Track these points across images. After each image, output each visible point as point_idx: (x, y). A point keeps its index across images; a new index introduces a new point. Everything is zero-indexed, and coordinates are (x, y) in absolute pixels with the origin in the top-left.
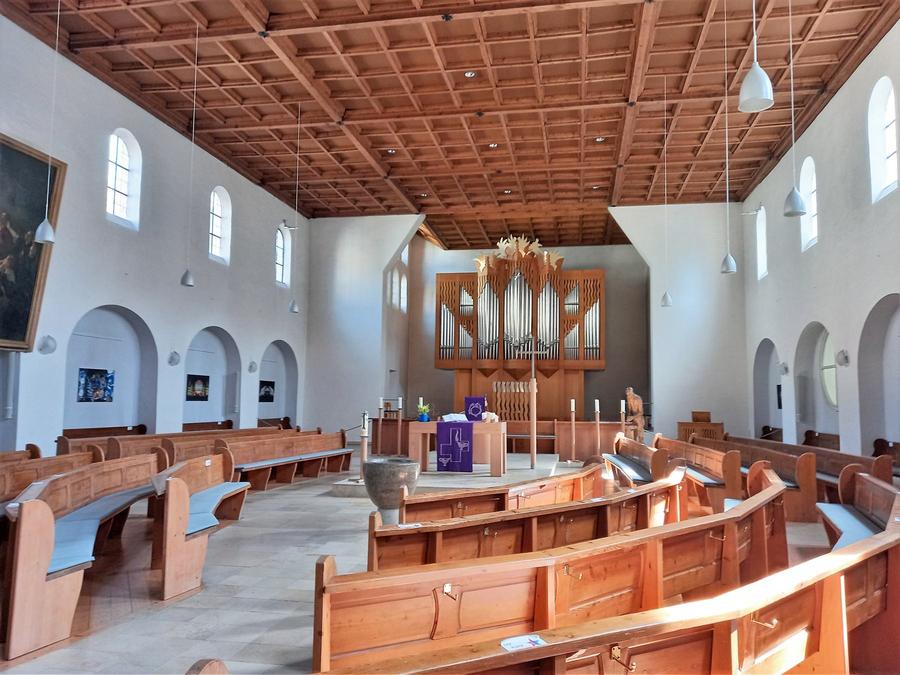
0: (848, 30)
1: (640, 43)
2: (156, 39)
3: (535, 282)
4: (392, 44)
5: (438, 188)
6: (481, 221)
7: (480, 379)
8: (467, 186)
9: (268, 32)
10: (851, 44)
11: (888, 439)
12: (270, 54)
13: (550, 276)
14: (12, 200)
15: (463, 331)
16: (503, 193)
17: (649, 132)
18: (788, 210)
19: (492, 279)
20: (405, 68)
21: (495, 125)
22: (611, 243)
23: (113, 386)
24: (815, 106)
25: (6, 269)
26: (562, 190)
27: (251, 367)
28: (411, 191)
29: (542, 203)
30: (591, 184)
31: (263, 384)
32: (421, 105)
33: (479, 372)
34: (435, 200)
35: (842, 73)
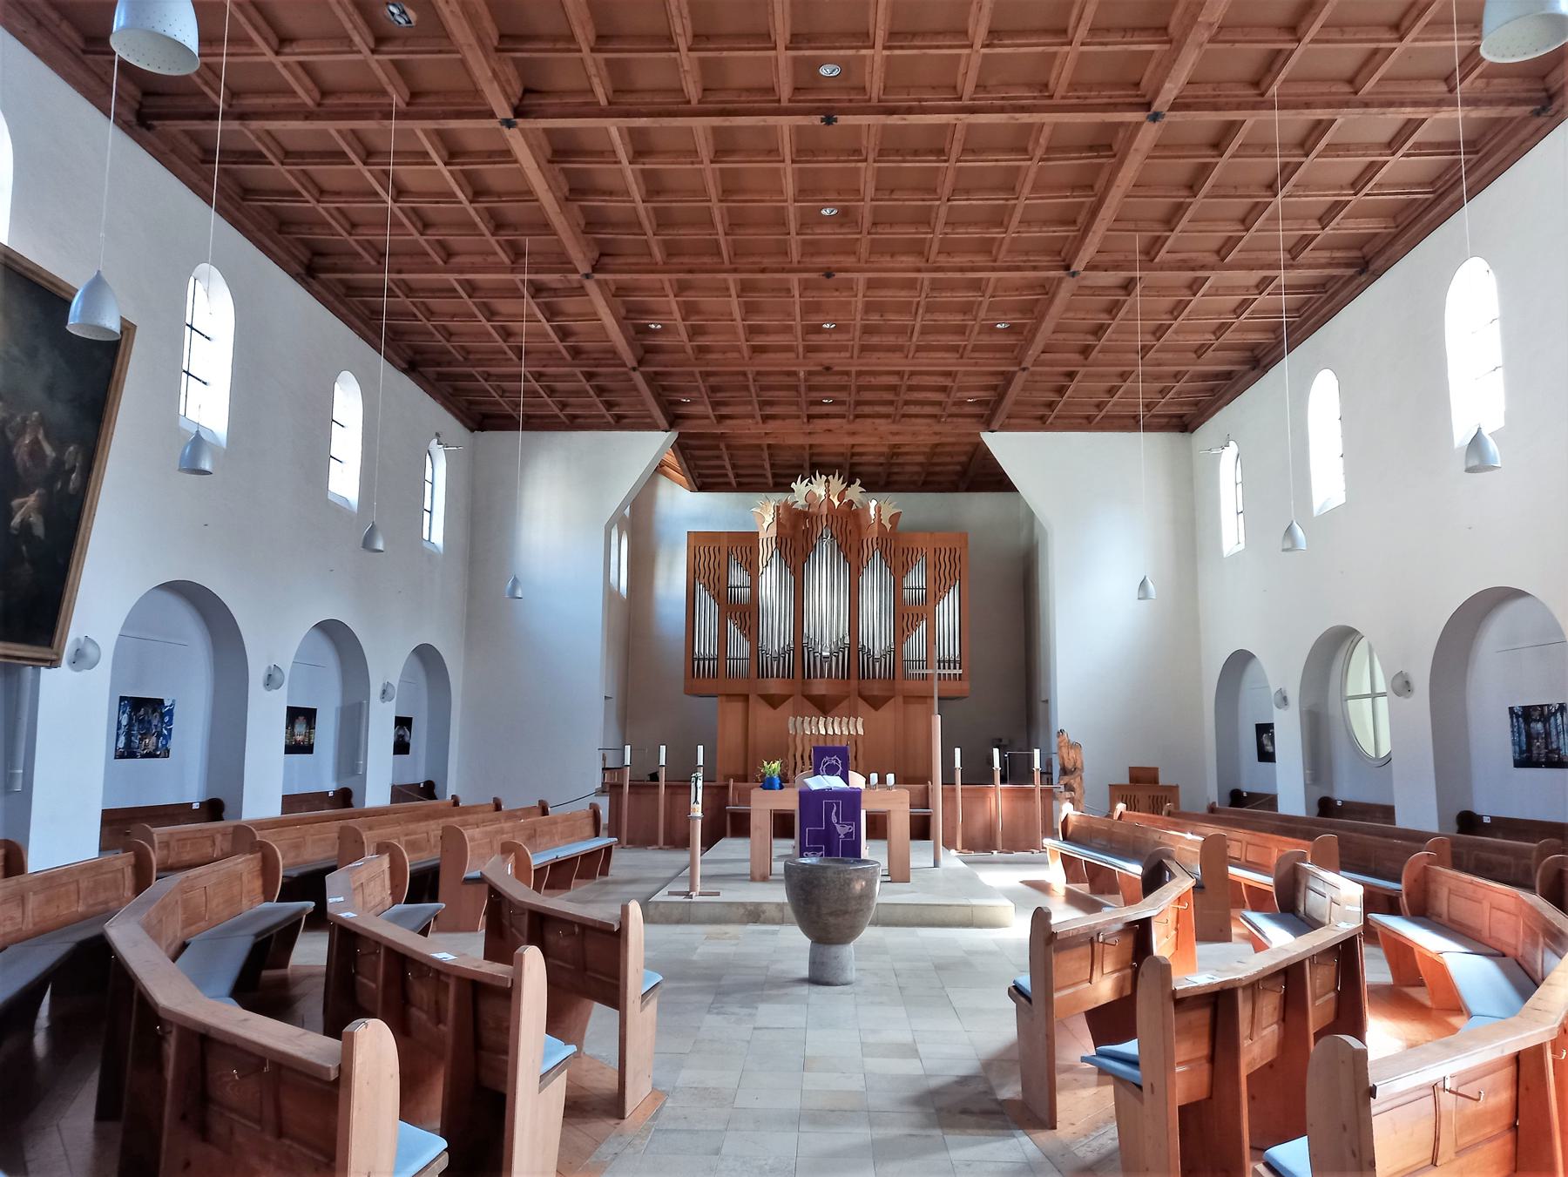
0: (1419, 185)
1: (1118, 182)
2: (309, 116)
3: (854, 550)
4: (719, 154)
5: (714, 389)
6: (769, 446)
7: (761, 712)
8: (763, 388)
9: (517, 120)
10: (1420, 205)
11: (1478, 810)
12: (506, 155)
13: (880, 541)
14: (50, 390)
17: (1084, 319)
18: (1474, 462)
20: (726, 193)
21: (844, 294)
22: (968, 490)
23: (171, 729)
24: (1344, 293)
25: (32, 515)
27: (384, 692)
28: (667, 393)
29: (877, 421)
31: (294, 714)
32: (732, 254)
33: (760, 699)
34: (705, 409)
35: (1398, 246)
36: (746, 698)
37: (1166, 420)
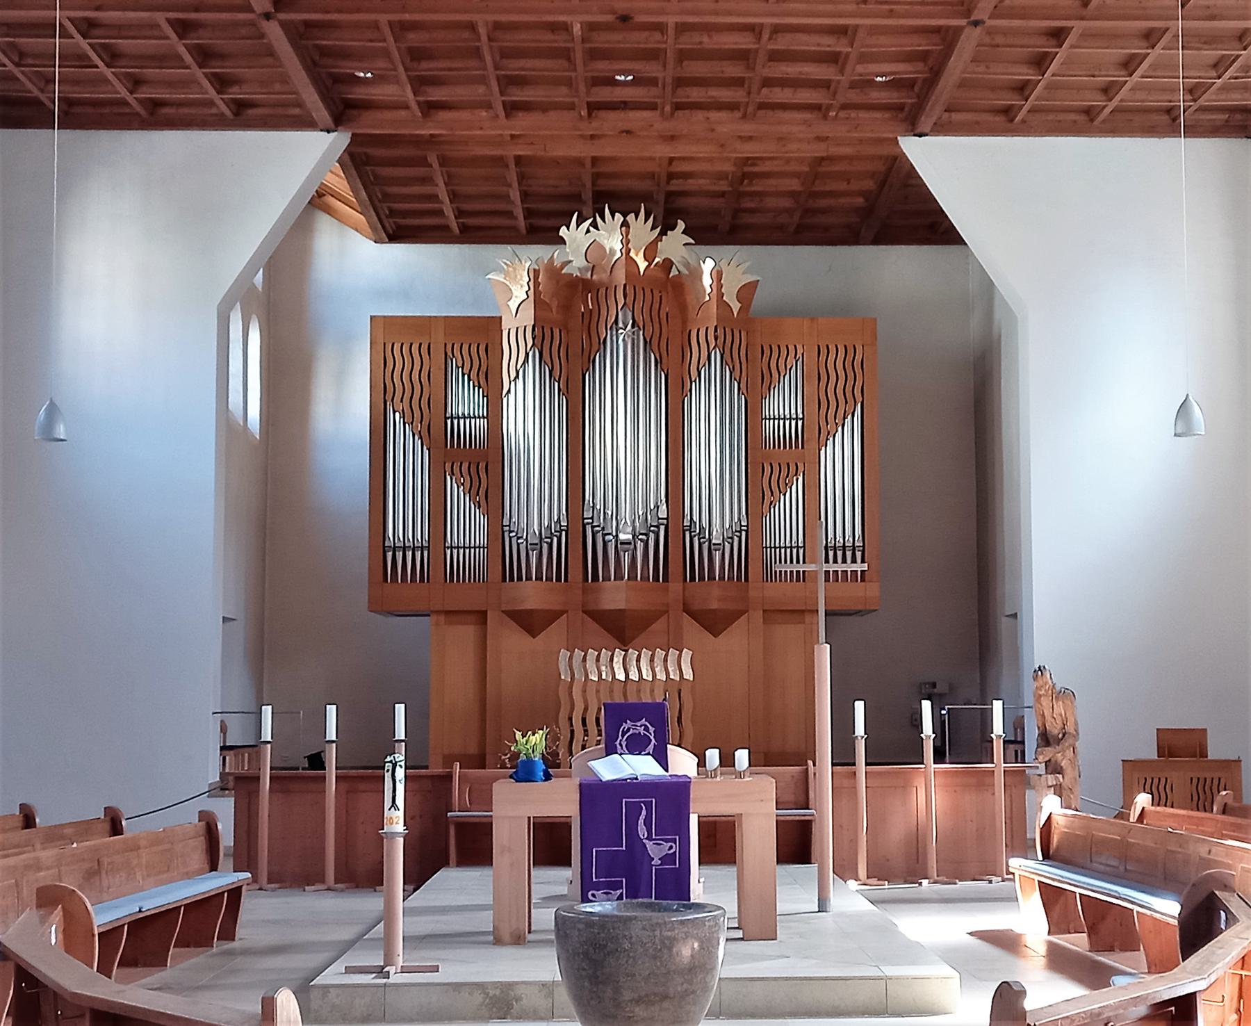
5: (416, 55)
6: (519, 160)
8: (506, 54)
15: (456, 493)
16: (612, 82)
19: (547, 335)
22: (876, 241)
26: (783, 83)
29: (714, 115)
30: (874, 68)
36: (481, 617)
37: (1224, 116)
